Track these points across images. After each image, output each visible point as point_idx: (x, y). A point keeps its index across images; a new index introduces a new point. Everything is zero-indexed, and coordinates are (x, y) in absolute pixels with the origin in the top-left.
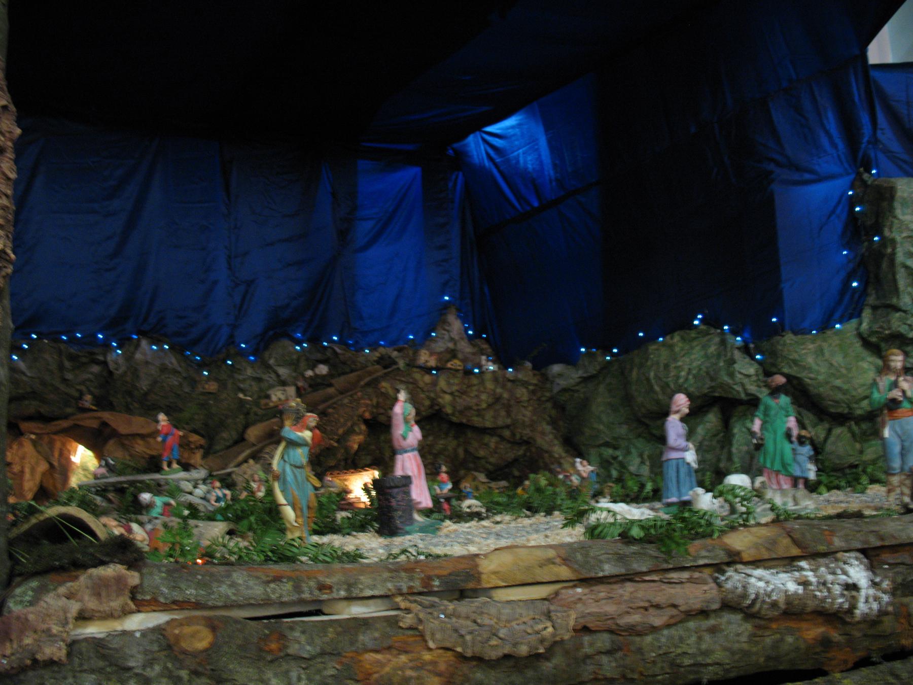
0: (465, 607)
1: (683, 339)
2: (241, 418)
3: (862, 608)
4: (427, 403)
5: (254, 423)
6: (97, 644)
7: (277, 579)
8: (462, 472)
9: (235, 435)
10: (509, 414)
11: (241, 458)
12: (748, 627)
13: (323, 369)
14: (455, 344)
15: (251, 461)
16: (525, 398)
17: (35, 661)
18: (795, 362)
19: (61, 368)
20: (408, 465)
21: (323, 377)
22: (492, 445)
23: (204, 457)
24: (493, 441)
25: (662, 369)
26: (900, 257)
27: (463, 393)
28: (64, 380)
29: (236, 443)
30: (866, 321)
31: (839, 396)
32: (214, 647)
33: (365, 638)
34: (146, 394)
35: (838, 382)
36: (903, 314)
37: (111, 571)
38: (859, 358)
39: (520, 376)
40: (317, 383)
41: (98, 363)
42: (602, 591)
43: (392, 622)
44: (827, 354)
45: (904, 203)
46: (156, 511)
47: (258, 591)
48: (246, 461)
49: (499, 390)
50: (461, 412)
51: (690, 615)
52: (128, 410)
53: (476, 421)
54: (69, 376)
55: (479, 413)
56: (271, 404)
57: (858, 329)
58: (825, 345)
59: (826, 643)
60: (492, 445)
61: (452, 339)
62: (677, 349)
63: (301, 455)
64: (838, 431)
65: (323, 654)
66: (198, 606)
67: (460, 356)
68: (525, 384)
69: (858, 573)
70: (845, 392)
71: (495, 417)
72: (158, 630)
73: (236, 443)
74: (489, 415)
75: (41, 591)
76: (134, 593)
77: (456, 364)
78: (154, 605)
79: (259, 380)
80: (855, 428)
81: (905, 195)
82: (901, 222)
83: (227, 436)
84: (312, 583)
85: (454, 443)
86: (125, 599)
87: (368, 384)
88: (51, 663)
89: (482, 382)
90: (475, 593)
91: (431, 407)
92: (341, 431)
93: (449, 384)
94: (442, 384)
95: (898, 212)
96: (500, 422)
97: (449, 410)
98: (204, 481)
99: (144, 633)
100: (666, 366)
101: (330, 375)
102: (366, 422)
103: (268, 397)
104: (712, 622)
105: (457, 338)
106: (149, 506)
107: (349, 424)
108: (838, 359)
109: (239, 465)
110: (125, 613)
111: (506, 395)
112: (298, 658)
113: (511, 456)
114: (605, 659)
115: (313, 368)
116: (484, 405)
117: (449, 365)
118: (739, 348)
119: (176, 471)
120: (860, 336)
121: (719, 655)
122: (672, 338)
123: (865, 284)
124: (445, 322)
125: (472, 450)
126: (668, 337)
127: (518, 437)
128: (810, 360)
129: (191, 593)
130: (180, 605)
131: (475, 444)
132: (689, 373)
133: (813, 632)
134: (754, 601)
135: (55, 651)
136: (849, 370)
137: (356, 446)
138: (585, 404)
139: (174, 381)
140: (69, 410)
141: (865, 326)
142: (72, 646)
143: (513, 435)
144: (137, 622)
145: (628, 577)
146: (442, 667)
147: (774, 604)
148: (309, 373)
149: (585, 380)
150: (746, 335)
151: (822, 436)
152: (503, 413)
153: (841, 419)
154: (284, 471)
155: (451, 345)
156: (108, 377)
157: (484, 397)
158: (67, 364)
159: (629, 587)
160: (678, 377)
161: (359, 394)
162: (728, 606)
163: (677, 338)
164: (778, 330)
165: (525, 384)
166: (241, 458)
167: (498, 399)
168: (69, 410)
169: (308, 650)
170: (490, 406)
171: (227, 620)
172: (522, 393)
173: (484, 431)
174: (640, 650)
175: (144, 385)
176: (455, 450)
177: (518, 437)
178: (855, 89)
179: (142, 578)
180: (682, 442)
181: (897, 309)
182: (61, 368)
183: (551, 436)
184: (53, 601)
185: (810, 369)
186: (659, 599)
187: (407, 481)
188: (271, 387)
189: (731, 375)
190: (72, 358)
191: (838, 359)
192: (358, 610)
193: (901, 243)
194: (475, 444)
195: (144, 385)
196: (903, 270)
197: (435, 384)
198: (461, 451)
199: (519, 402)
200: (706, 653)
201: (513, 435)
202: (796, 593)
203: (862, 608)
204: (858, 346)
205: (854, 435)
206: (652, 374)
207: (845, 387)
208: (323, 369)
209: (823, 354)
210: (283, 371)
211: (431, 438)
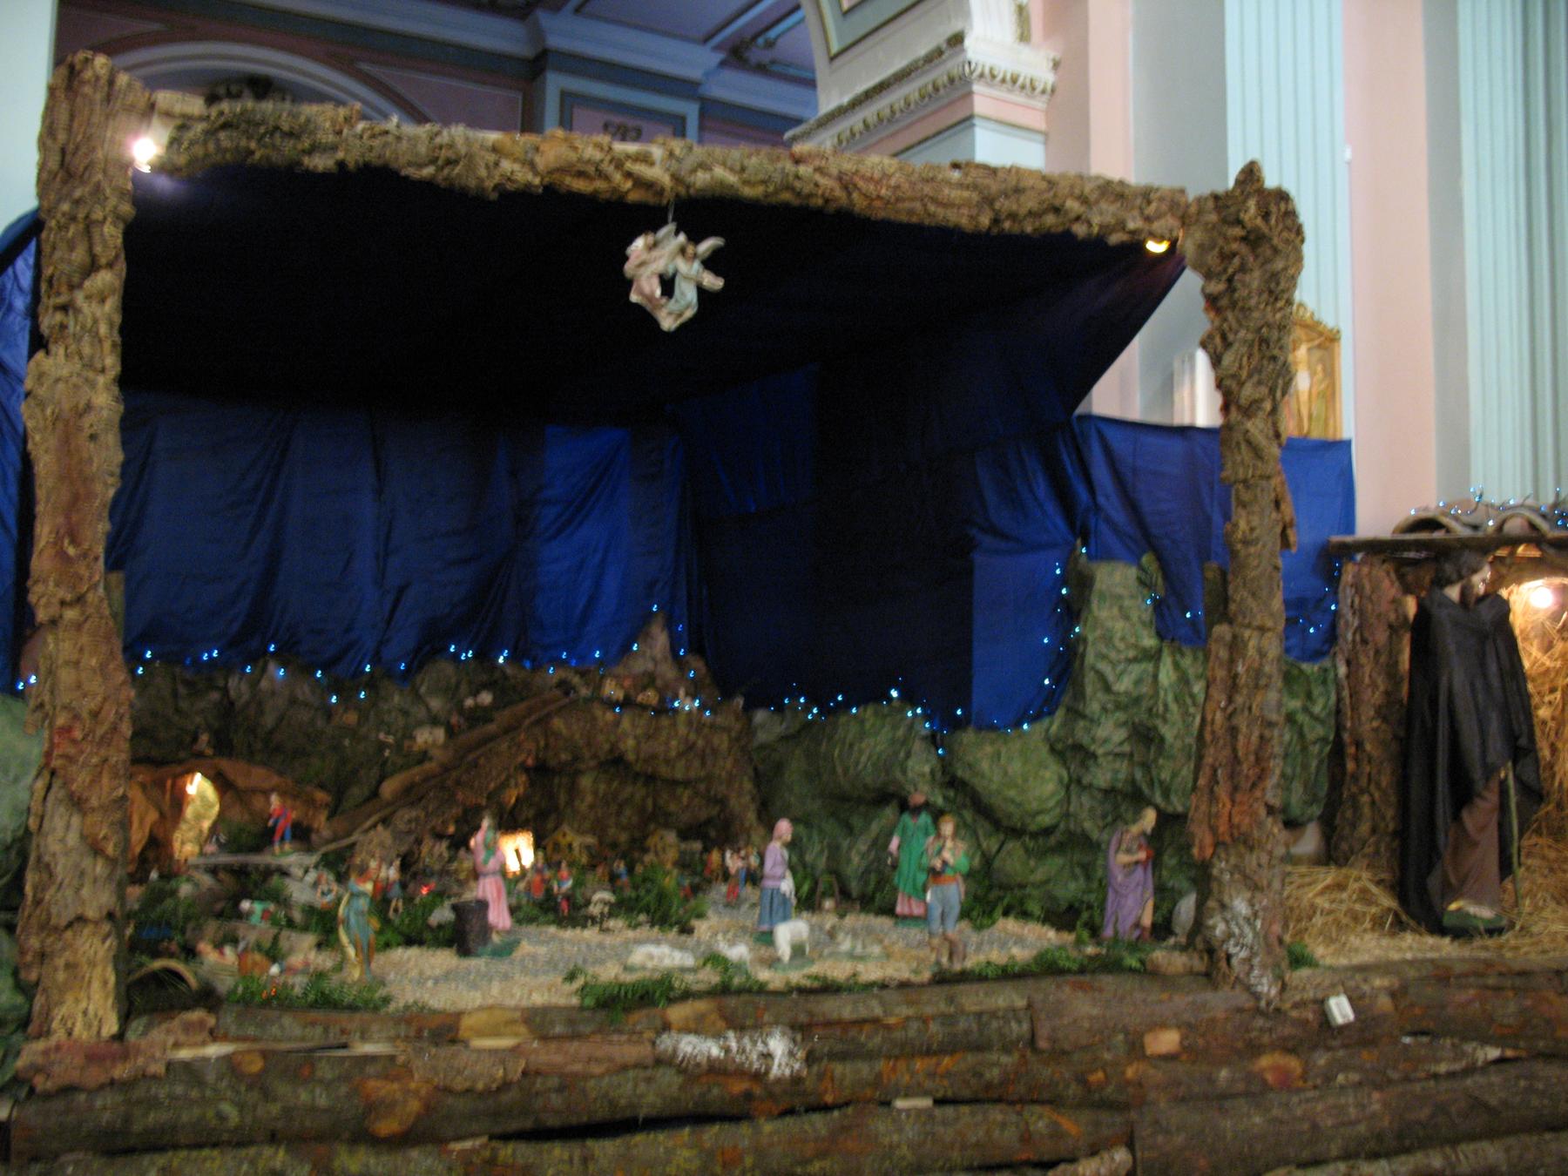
0: (445, 1051)
1: (876, 714)
2: (375, 772)
3: (775, 1071)
4: (607, 747)
5: (392, 774)
6: (187, 1066)
7: (313, 1024)
8: (652, 827)
9: (366, 792)
10: (703, 764)
11: (369, 823)
12: (679, 1080)
13: (486, 698)
14: (656, 665)
15: (380, 828)
16: (725, 746)
17: (144, 1076)
18: (970, 766)
19: (175, 694)
20: (488, 888)
21: (485, 709)
22: (685, 800)
23: (329, 818)
24: (685, 795)
25: (847, 746)
26: (1090, 658)
27: (649, 737)
28: (177, 710)
29: (368, 800)
30: (1055, 724)
31: (1012, 808)
32: (264, 1071)
33: (370, 1069)
34: (271, 732)
35: (1012, 793)
36: (1087, 724)
37: (196, 1015)
38: (1042, 765)
39: (720, 720)
40: (477, 717)
41: (217, 688)
42: (553, 1046)
43: (392, 1058)
44: (1003, 761)
45: (1102, 596)
46: (255, 919)
47: (298, 1032)
48: (374, 826)
49: (692, 736)
50: (646, 761)
51: (624, 1068)
52: (250, 756)
53: (664, 770)
54: (184, 705)
55: (667, 762)
56: (415, 749)
57: (1047, 730)
58: (1004, 750)
59: (748, 1096)
60: (685, 800)
61: (654, 659)
62: (868, 725)
63: (363, 904)
64: (1010, 845)
65: (339, 1078)
66: (255, 1039)
67: (659, 682)
68: (727, 730)
69: (778, 1045)
70: (1019, 805)
71: (688, 768)
72: (227, 1058)
73: (368, 800)
74: (681, 764)
75: (148, 1027)
76: (211, 1032)
77: (650, 697)
78: (225, 1038)
79: (406, 713)
80: (1031, 844)
81: (1104, 587)
82: (1096, 618)
83: (357, 792)
84: (338, 1027)
85: (643, 792)
86: (205, 1034)
87: (538, 722)
88: (154, 1077)
89: (674, 725)
90: (453, 1041)
91: (611, 751)
92: (492, 785)
93: (633, 725)
94: (626, 724)
95: (1094, 605)
96: (692, 774)
97: (631, 757)
98: (316, 867)
99: (218, 1059)
100: (851, 746)
101: (495, 706)
102: (527, 770)
103: (413, 738)
104: (649, 1073)
105: (659, 656)
106: (249, 914)
107: (503, 777)
108: (1016, 767)
109: (367, 831)
110: (204, 1044)
111: (700, 743)
112: (321, 1081)
113: (703, 815)
114: (553, 1096)
115: (475, 694)
116: (673, 753)
117: (640, 698)
118: (924, 738)
119: (288, 854)
120: (1047, 739)
121: (651, 1098)
122: (865, 711)
123: (1057, 680)
124: (648, 635)
125: (661, 802)
126: (862, 709)
127: (712, 793)
128: (985, 766)
129: (251, 1031)
130: (244, 1039)
131: (665, 796)
132: (869, 759)
133: (738, 1087)
134: (682, 1061)
135: (157, 1068)
136: (1026, 780)
137: (513, 801)
138: (779, 767)
139: (304, 716)
140: (182, 755)
141: (1054, 728)
142: (170, 1065)
143: (708, 790)
144: (214, 1050)
145: (576, 1036)
146: (423, 1092)
147: (698, 1065)
148: (469, 702)
149: (785, 738)
150: (937, 721)
151: (994, 848)
152: (697, 763)
153: (1016, 832)
154: (348, 917)
155: (650, 666)
156: (228, 708)
157: (674, 743)
158: (182, 690)
159: (576, 1044)
160: (857, 763)
161: (522, 737)
162: (659, 1061)
163: (870, 710)
164: (958, 725)
165: (727, 730)
166: (369, 823)
167: (691, 747)
168: (182, 755)
169: (329, 1075)
170: (680, 755)
171: (274, 1052)
172: (722, 741)
173: (674, 783)
174: (584, 1091)
175: (269, 720)
176: (644, 799)
177: (712, 793)
178: (1065, 457)
179: (218, 1019)
180: (779, 870)
181: (1084, 717)
182: (175, 694)
183: (748, 798)
184: (157, 1035)
185: (983, 776)
186: (599, 1053)
187: (483, 905)
188: (420, 724)
189: (904, 772)
190: (189, 684)
191: (1016, 767)
192: (369, 1048)
193: (1094, 644)
194: (665, 796)
195: (269, 720)
196: (1092, 673)
197: (617, 723)
198: (650, 802)
199: (715, 751)
200: (642, 1096)
201: (708, 790)
202: (718, 1058)
203: (775, 1071)
204: (1044, 751)
205: (1027, 850)
206: (836, 753)
207: (1018, 799)
208: (486, 698)
209: (999, 759)
210: (436, 704)
211: (615, 784)
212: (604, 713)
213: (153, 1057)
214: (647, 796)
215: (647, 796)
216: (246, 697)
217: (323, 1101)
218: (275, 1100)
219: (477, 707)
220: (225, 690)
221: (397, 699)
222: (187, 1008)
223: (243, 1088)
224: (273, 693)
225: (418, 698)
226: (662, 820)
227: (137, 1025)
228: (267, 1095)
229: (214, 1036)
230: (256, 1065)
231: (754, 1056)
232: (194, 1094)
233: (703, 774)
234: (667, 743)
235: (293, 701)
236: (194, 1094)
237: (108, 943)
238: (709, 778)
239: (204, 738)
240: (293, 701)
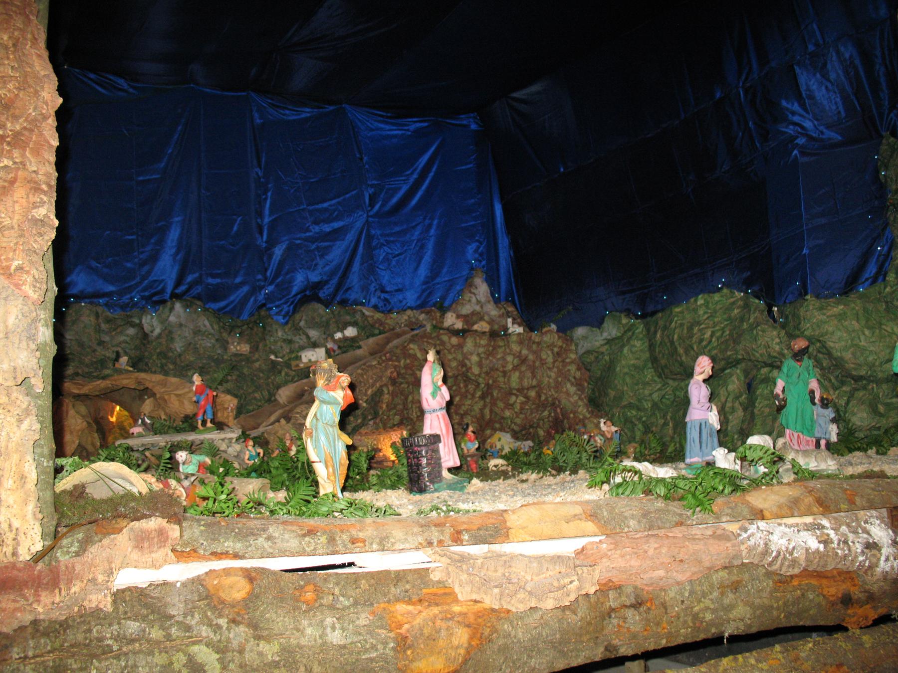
7: (311, 532)
13: (351, 332)
16: (550, 360)
19: (98, 330)
21: (353, 340)
37: (154, 523)
41: (133, 325)
48: (278, 421)
61: (478, 302)
71: (521, 379)
72: (197, 581)
74: (515, 377)
89: (508, 345)
96: (526, 384)
103: (299, 358)
105: (483, 300)
111: (531, 357)
116: (510, 367)
140: (107, 372)
148: (338, 335)
170: (515, 368)
171: (263, 571)
188: (302, 348)
198: (487, 411)
200: (731, 607)
202: (818, 550)
208: (351, 332)
212: (450, 338)
213: (93, 581)
214: (485, 406)
215: (485, 406)
216: (157, 331)
217: (336, 637)
218: (268, 639)
219: (345, 339)
220: (140, 326)
221: (280, 334)
222: (138, 517)
223: (223, 622)
224: (181, 325)
225: (297, 329)
226: (497, 426)
227: (71, 543)
228: (258, 632)
229: (182, 554)
230: (239, 590)
231: (859, 548)
232: (156, 634)
233: (534, 383)
234: (503, 358)
235: (197, 332)
236: (156, 634)
237: (25, 425)
238: (539, 387)
239: (124, 360)
240: (197, 332)
